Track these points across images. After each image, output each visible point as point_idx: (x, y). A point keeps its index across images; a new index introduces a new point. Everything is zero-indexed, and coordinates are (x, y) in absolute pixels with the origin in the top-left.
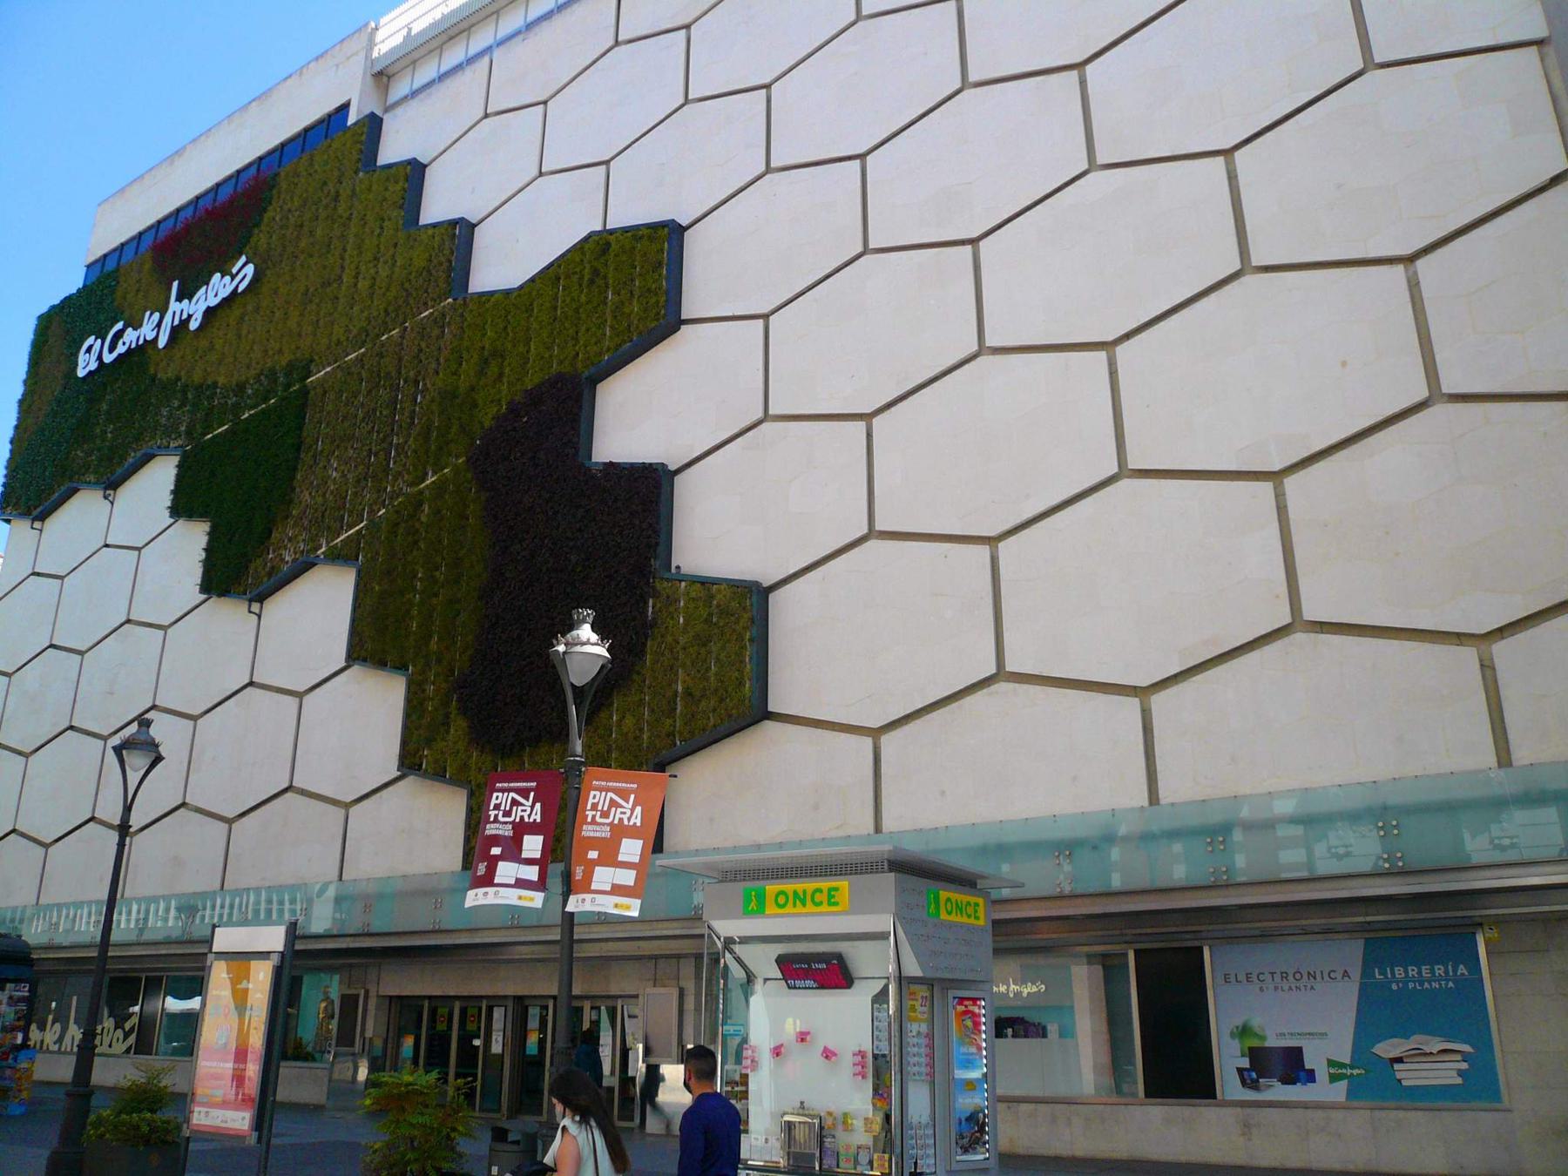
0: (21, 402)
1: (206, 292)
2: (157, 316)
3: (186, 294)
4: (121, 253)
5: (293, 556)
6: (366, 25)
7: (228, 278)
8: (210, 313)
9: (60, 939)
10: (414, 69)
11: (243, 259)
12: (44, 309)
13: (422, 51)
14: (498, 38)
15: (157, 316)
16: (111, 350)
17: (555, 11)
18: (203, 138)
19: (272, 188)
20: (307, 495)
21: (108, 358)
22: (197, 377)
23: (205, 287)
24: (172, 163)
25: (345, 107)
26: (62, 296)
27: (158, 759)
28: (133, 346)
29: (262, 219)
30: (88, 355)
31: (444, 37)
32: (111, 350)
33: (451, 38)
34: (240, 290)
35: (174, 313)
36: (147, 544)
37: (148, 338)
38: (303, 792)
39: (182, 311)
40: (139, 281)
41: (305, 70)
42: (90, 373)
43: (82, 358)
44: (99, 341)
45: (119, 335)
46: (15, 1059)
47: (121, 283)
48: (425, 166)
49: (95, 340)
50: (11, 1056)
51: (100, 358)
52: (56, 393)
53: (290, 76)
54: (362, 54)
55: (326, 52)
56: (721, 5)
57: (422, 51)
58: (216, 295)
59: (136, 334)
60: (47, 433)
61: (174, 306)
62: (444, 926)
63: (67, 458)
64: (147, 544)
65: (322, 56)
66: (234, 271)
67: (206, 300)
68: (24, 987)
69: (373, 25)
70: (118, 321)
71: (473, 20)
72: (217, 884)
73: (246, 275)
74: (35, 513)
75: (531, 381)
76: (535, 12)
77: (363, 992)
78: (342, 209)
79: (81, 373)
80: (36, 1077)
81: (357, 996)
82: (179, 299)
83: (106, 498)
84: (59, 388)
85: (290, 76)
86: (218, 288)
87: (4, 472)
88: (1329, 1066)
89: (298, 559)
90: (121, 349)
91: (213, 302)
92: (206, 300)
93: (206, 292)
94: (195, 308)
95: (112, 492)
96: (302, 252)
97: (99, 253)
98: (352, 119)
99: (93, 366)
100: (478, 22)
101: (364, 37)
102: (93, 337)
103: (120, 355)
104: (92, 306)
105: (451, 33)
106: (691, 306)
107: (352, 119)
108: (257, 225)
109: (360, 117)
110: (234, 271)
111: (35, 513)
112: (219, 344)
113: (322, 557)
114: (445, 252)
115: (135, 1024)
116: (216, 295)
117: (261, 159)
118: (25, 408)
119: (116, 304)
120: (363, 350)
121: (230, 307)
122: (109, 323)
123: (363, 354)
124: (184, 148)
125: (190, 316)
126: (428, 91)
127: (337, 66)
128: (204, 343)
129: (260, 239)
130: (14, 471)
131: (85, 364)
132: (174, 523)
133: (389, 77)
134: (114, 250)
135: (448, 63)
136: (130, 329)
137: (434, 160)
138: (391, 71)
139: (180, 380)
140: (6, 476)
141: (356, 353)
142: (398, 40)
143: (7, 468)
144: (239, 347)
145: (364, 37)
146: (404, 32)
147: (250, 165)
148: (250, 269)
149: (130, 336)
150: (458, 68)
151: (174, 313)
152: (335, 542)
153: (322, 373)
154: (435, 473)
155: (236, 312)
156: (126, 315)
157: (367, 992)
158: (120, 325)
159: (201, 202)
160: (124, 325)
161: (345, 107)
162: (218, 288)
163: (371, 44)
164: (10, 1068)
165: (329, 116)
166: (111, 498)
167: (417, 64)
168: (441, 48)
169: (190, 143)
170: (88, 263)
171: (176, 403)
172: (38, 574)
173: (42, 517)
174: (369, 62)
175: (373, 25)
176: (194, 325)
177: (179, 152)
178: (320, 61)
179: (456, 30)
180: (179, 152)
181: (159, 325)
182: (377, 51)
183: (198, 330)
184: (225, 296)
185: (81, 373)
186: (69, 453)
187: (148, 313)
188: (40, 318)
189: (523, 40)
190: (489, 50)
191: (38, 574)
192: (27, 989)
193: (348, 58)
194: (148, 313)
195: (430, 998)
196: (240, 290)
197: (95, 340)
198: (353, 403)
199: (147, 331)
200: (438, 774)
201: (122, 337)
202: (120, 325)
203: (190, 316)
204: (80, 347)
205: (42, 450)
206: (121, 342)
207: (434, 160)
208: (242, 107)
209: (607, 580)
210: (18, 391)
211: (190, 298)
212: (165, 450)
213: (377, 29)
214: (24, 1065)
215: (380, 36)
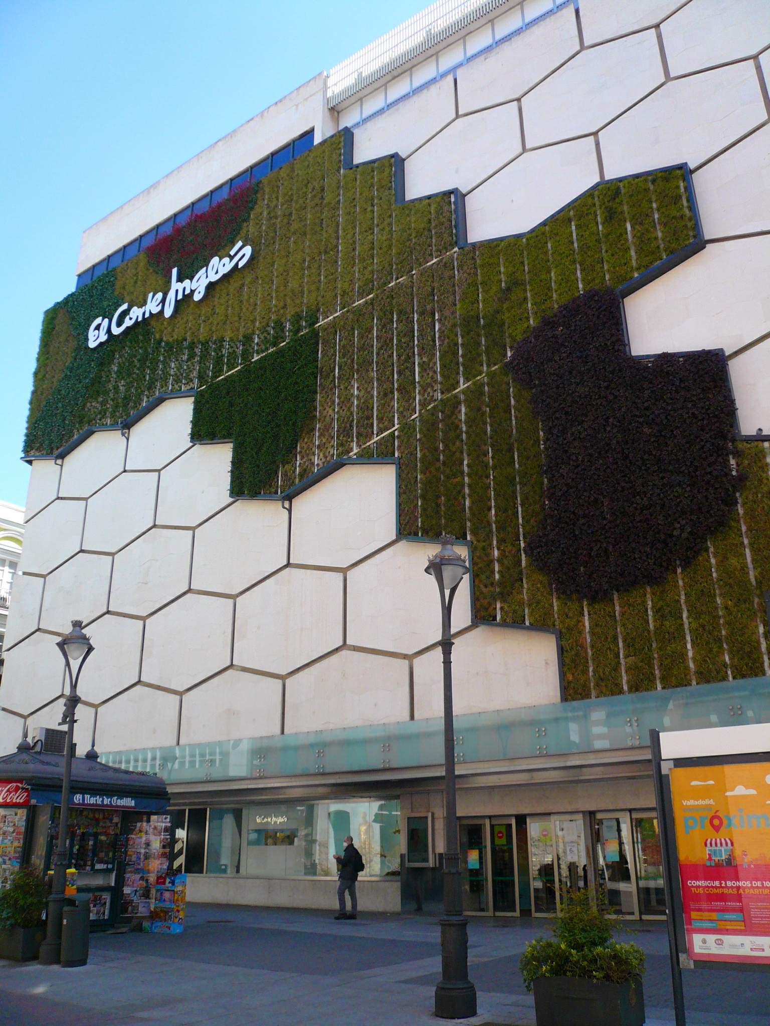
0: (36, 374)
1: (207, 271)
2: (160, 296)
3: (186, 275)
4: (93, 271)
5: (323, 460)
6: (320, 74)
7: (226, 260)
8: (211, 287)
9: (216, 773)
10: (386, 90)
11: (240, 244)
12: (50, 305)
13: (420, 59)
14: (440, 72)
15: (160, 296)
16: (119, 324)
17: (386, 109)
18: (176, 172)
19: (257, 192)
20: (331, 412)
21: (116, 331)
22: (203, 334)
23: (205, 268)
24: (149, 193)
25: (310, 133)
26: (65, 295)
27: (90, 649)
28: (140, 319)
29: (249, 216)
30: (97, 331)
31: (389, 77)
32: (119, 324)
33: (394, 78)
34: (240, 266)
35: (177, 291)
36: (92, 496)
37: (154, 312)
38: (356, 649)
39: (184, 289)
40: (136, 275)
41: (265, 113)
42: (101, 344)
43: (92, 334)
44: (106, 320)
45: (125, 313)
46: (173, 883)
47: (119, 278)
48: (404, 160)
49: (103, 320)
50: (168, 880)
51: (109, 331)
52: (67, 364)
53: (252, 119)
54: (320, 96)
55: (285, 97)
56: (690, 3)
57: (420, 59)
58: (217, 272)
59: (141, 311)
60: (63, 392)
61: (175, 286)
62: (394, 765)
63: (83, 409)
64: (92, 496)
65: (280, 101)
66: (232, 253)
67: (207, 277)
68: (166, 818)
69: (325, 74)
70: (124, 303)
71: (415, 61)
72: (278, 730)
73: (244, 255)
74: (56, 453)
75: (556, 299)
76: (532, 12)
77: (430, 815)
78: (328, 197)
79: (92, 344)
80: (188, 899)
81: (426, 818)
82: (180, 279)
83: (123, 435)
84: (69, 360)
85: (252, 119)
86: (218, 267)
87: (26, 425)
88: (470, 876)
89: (329, 461)
90: (128, 323)
91: (214, 278)
92: (207, 277)
93: (207, 271)
94: (199, 285)
95: (127, 431)
96: (294, 233)
97: (89, 265)
98: (317, 139)
99: (103, 338)
100: (419, 64)
101: (320, 83)
102: (100, 319)
103: (128, 328)
104: (95, 298)
105: (395, 73)
106: (710, 229)
107: (317, 139)
108: (246, 220)
109: (325, 138)
110: (232, 253)
111: (56, 453)
112: (220, 310)
113: (355, 457)
114: (444, 215)
115: (183, 847)
116: (217, 272)
117: (231, 180)
118: (40, 376)
119: (116, 293)
120: (371, 296)
121: (229, 282)
122: (113, 307)
123: (372, 299)
124: (158, 182)
125: (192, 292)
126: (395, 107)
127: (297, 105)
128: (205, 310)
129: (251, 228)
130: (36, 423)
131: (96, 338)
132: (193, 446)
133: (338, 113)
134: (104, 260)
135: (502, 32)
136: (135, 308)
137: (410, 156)
138: (339, 108)
139: (186, 340)
140: (27, 428)
141: (364, 300)
142: (350, 81)
143: (28, 422)
144: (241, 309)
145: (320, 83)
146: (356, 75)
147: (221, 187)
148: (248, 250)
149: (136, 313)
150: (507, 38)
151: (177, 291)
152: (368, 444)
153: (331, 318)
154: (467, 379)
155: (234, 284)
156: (127, 298)
157: (433, 814)
158: (125, 307)
159: (161, 230)
160: (129, 305)
161: (310, 133)
162: (218, 267)
163: (325, 88)
164: (168, 890)
165: (294, 141)
166: (126, 435)
167: (439, 54)
168: (385, 85)
169: (163, 178)
170: (78, 273)
171: (185, 357)
172: (62, 498)
173: (62, 456)
174: (326, 101)
175: (325, 74)
176: (197, 297)
177: (154, 186)
178: (279, 105)
179: (399, 70)
180: (154, 186)
181: (163, 301)
182: (331, 92)
183: (201, 301)
184: (129, 325)
185: (92, 344)
186: (85, 405)
187: (151, 295)
188: (47, 313)
189: (485, 59)
190: (453, 70)
191: (62, 498)
192: (168, 820)
193: (306, 99)
194: (151, 295)
195: (490, 817)
196: (240, 266)
197: (103, 320)
198: (367, 337)
199: (152, 306)
200: (515, 622)
201: (129, 314)
202: (125, 307)
203: (192, 292)
204: (89, 325)
205: (60, 405)
206: (128, 318)
207: (410, 156)
208: (211, 146)
209: (688, 445)
210: (33, 366)
211: (191, 279)
212: (178, 394)
213: (328, 77)
214: (180, 888)
215: (330, 82)
